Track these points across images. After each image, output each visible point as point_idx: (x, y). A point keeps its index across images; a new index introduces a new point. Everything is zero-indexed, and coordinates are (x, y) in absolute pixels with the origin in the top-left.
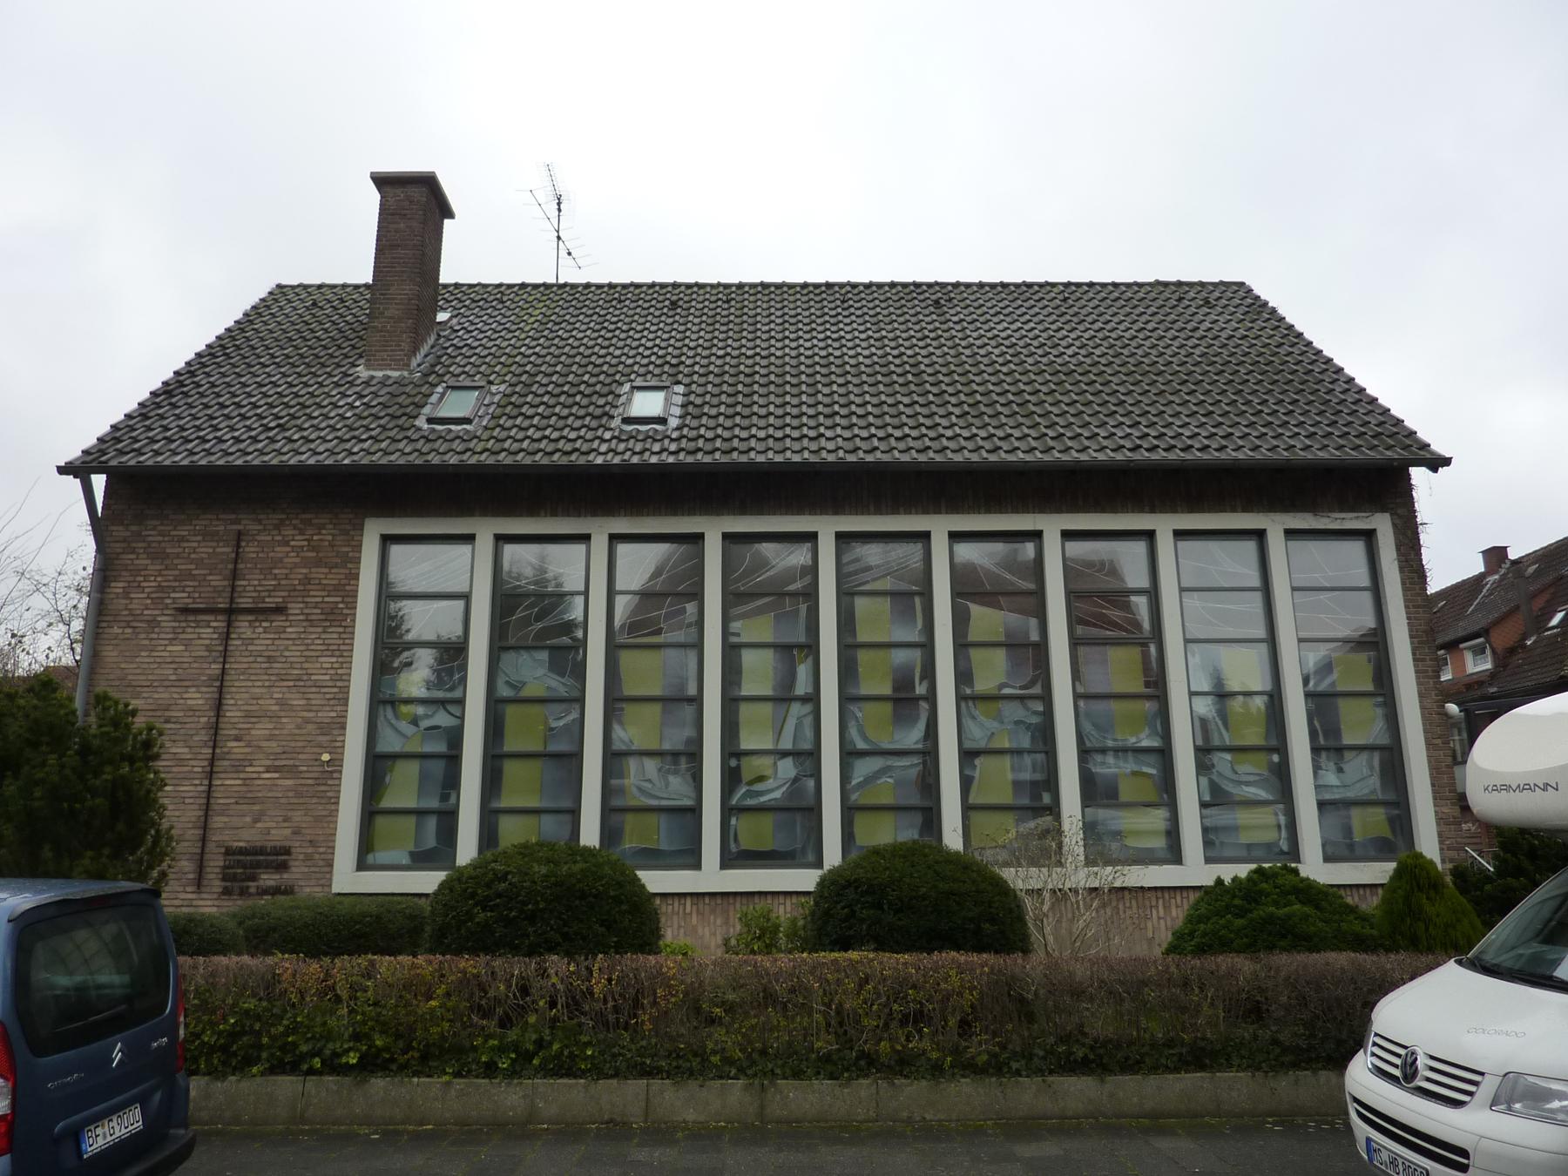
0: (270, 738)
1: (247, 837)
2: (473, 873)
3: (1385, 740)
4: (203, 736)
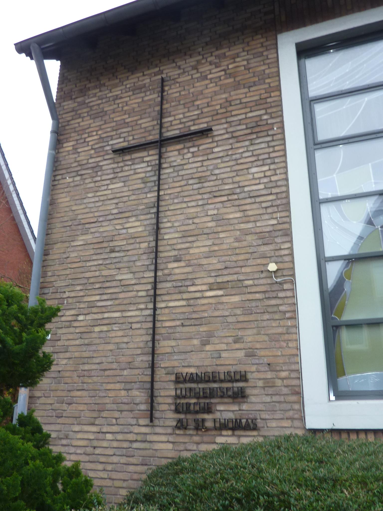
1: (196, 362)
4: (146, 261)
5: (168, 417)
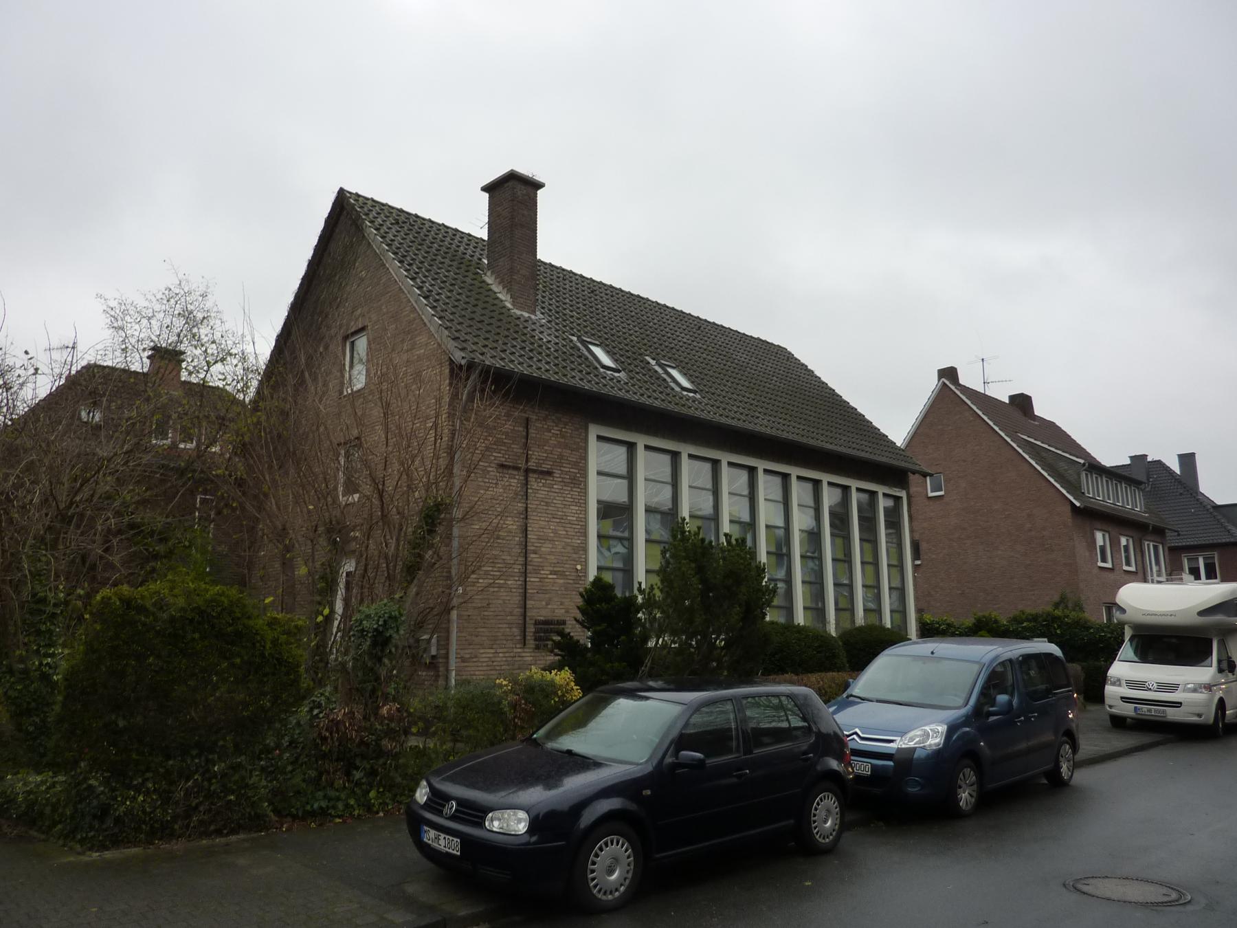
0: (551, 553)
1: (543, 614)
2: (753, 565)
3: (899, 585)
4: (517, 550)
5: (531, 642)
